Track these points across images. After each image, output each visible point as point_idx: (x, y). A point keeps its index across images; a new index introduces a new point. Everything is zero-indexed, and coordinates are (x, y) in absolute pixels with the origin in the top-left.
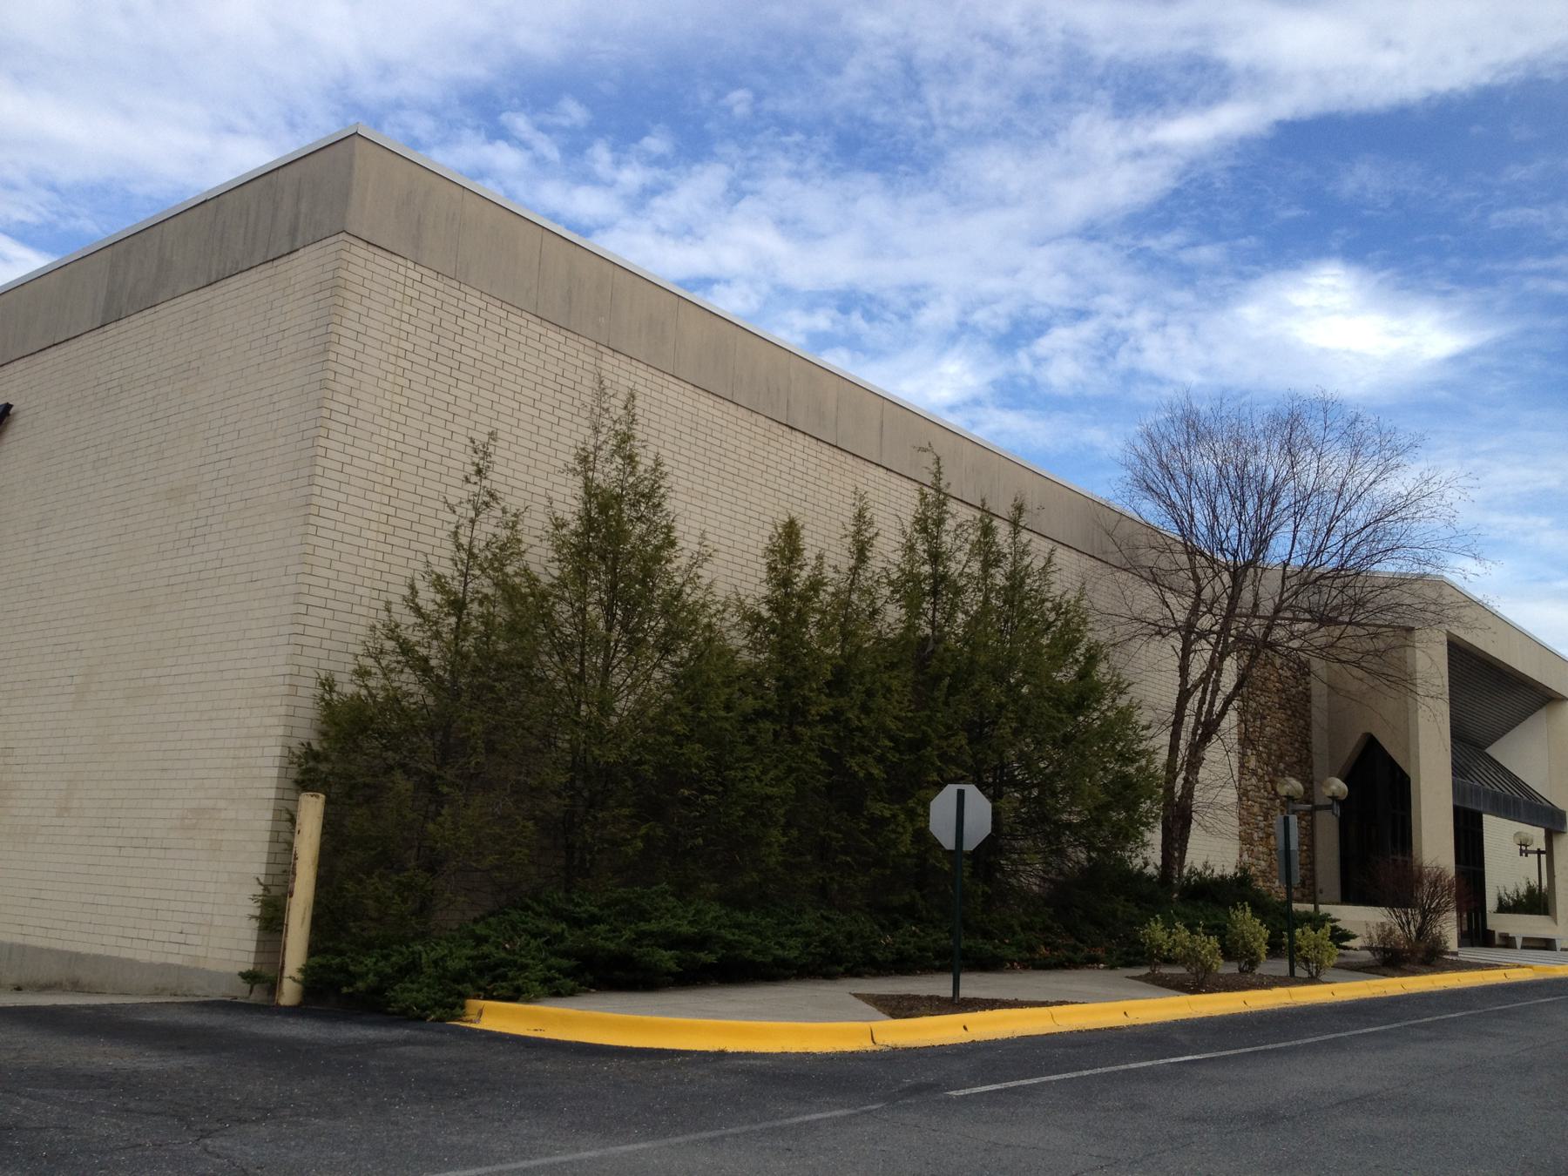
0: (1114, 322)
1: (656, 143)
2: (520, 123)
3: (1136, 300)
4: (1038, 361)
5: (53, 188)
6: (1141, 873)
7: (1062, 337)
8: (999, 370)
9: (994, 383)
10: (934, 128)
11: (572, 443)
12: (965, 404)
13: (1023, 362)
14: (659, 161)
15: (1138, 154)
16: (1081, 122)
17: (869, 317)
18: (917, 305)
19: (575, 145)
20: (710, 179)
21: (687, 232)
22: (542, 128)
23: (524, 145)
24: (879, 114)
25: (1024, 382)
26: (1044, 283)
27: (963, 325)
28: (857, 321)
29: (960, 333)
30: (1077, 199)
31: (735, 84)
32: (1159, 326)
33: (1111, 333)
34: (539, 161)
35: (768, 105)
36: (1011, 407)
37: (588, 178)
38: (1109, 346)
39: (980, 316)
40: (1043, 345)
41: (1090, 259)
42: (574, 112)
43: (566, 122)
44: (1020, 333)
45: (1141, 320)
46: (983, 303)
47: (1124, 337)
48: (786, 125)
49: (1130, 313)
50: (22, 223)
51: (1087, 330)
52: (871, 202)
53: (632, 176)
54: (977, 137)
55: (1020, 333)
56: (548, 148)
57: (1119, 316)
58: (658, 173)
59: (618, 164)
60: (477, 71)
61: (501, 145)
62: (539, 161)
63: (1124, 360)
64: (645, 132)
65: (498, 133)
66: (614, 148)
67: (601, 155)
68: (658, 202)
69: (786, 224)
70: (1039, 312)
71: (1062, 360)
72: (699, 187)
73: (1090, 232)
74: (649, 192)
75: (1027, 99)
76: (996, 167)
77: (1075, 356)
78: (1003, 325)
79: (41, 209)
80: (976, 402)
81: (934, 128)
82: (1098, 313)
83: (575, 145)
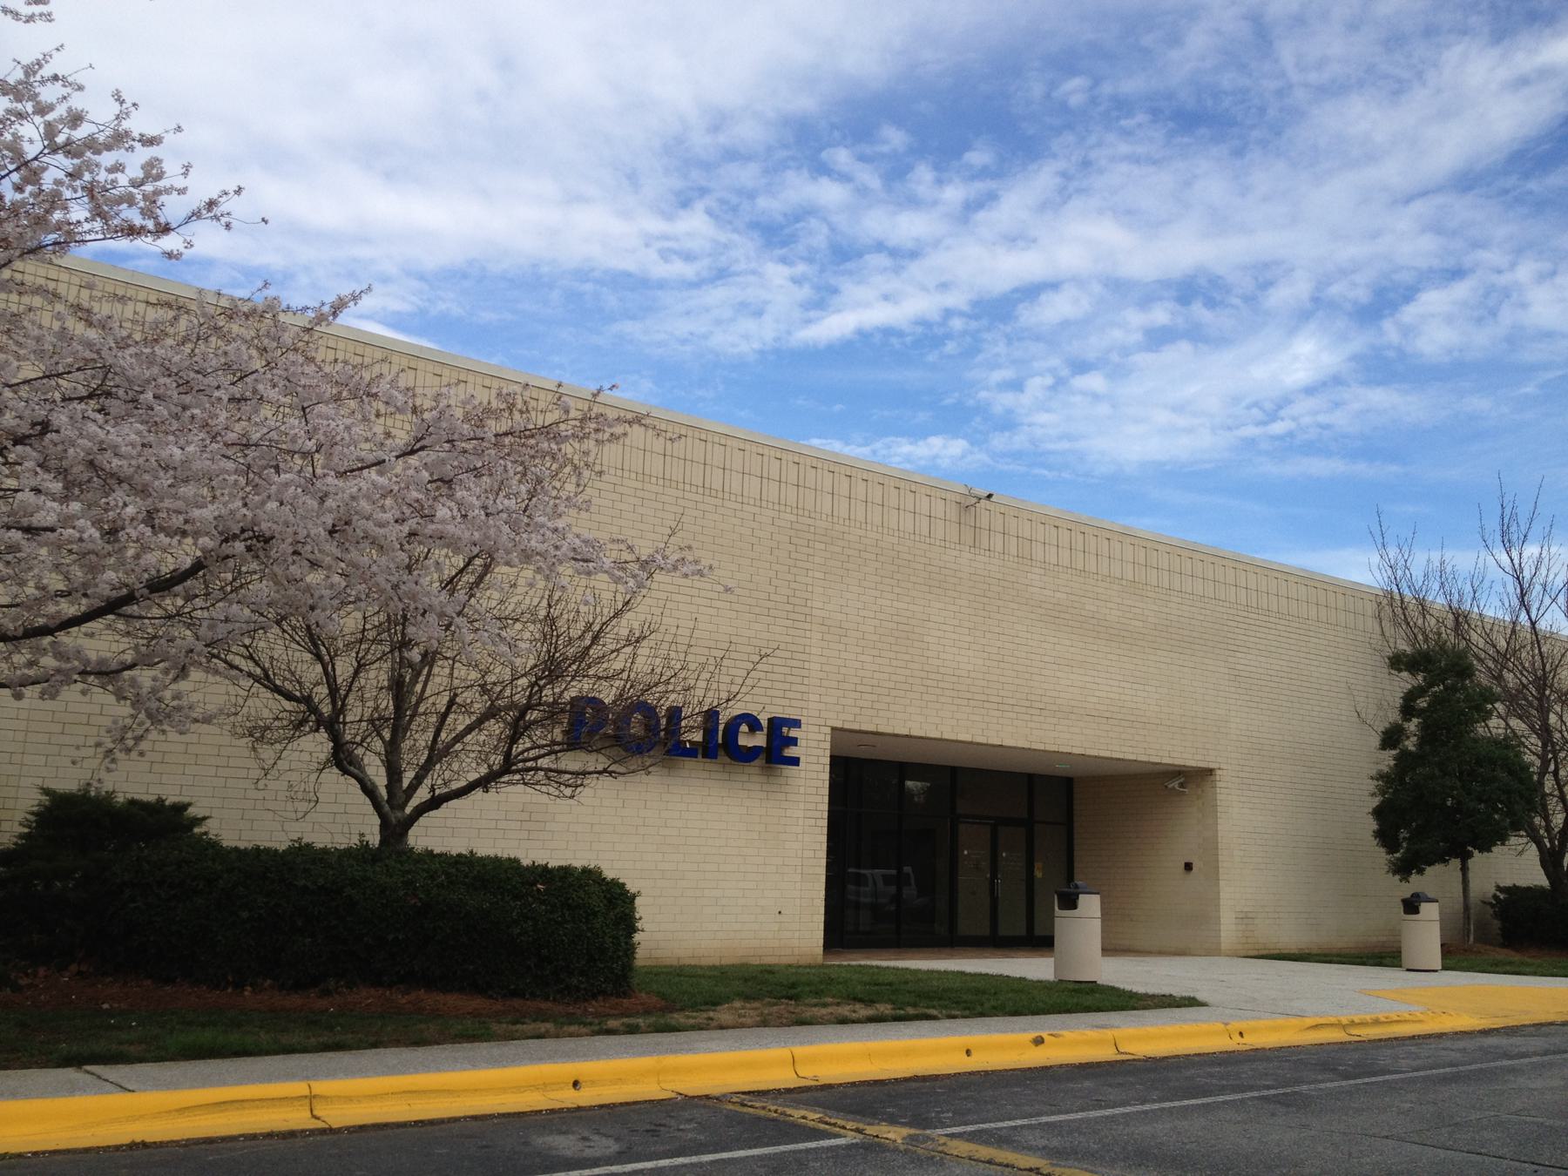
0: (1495, 278)
1: (978, 157)
2: (842, 157)
3: (1519, 251)
4: (1407, 331)
5: (421, 277)
6: (97, 797)
7: (1434, 300)
8: (1359, 342)
9: (1355, 358)
10: (1291, 86)
11: (654, 594)
12: (1324, 384)
13: (1390, 331)
14: (983, 173)
15: (1523, 82)
16: (1452, 55)
17: (1211, 303)
18: (1266, 285)
19: (896, 171)
20: (1044, 178)
21: (1015, 239)
22: (862, 158)
23: (844, 178)
24: (1228, 80)
25: (1391, 354)
26: (1409, 244)
27: (1316, 300)
28: (1198, 310)
29: (1317, 308)
30: (1451, 147)
31: (1072, 72)
32: (1543, 277)
33: (1489, 290)
34: (862, 191)
35: (1107, 89)
36: (1379, 383)
37: (913, 202)
38: (1489, 304)
39: (1335, 290)
40: (1409, 313)
41: (1464, 209)
42: (895, 138)
43: (885, 149)
44: (1386, 299)
45: (1525, 272)
46: (1343, 272)
47: (1506, 293)
48: (1122, 106)
49: (1513, 266)
50: (398, 313)
51: (1461, 290)
52: (1212, 181)
53: (954, 194)
54: (1334, 90)
55: (1386, 299)
56: (870, 178)
57: (1499, 272)
58: (980, 186)
59: (940, 182)
60: (805, 104)
61: (824, 181)
62: (862, 191)
63: (1507, 317)
64: (967, 147)
65: (822, 170)
66: (937, 167)
67: (923, 175)
68: (981, 215)
69: (1128, 215)
70: (1405, 277)
71: (1435, 324)
72: (1017, 201)
73: (1466, 181)
74: (972, 207)
75: (1394, 41)
76: (1362, 117)
77: (1449, 319)
78: (1362, 295)
79: (414, 299)
80: (1336, 381)
81: (1291, 86)
82: (1472, 270)
83: (896, 171)
